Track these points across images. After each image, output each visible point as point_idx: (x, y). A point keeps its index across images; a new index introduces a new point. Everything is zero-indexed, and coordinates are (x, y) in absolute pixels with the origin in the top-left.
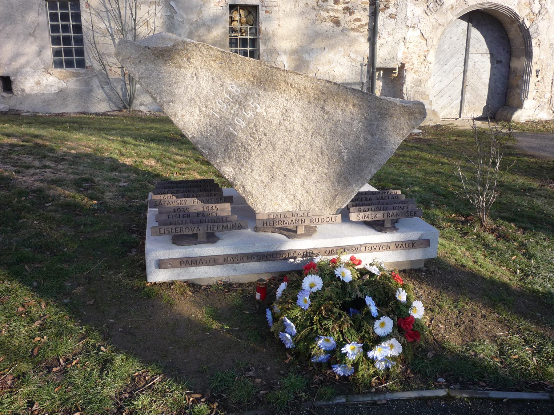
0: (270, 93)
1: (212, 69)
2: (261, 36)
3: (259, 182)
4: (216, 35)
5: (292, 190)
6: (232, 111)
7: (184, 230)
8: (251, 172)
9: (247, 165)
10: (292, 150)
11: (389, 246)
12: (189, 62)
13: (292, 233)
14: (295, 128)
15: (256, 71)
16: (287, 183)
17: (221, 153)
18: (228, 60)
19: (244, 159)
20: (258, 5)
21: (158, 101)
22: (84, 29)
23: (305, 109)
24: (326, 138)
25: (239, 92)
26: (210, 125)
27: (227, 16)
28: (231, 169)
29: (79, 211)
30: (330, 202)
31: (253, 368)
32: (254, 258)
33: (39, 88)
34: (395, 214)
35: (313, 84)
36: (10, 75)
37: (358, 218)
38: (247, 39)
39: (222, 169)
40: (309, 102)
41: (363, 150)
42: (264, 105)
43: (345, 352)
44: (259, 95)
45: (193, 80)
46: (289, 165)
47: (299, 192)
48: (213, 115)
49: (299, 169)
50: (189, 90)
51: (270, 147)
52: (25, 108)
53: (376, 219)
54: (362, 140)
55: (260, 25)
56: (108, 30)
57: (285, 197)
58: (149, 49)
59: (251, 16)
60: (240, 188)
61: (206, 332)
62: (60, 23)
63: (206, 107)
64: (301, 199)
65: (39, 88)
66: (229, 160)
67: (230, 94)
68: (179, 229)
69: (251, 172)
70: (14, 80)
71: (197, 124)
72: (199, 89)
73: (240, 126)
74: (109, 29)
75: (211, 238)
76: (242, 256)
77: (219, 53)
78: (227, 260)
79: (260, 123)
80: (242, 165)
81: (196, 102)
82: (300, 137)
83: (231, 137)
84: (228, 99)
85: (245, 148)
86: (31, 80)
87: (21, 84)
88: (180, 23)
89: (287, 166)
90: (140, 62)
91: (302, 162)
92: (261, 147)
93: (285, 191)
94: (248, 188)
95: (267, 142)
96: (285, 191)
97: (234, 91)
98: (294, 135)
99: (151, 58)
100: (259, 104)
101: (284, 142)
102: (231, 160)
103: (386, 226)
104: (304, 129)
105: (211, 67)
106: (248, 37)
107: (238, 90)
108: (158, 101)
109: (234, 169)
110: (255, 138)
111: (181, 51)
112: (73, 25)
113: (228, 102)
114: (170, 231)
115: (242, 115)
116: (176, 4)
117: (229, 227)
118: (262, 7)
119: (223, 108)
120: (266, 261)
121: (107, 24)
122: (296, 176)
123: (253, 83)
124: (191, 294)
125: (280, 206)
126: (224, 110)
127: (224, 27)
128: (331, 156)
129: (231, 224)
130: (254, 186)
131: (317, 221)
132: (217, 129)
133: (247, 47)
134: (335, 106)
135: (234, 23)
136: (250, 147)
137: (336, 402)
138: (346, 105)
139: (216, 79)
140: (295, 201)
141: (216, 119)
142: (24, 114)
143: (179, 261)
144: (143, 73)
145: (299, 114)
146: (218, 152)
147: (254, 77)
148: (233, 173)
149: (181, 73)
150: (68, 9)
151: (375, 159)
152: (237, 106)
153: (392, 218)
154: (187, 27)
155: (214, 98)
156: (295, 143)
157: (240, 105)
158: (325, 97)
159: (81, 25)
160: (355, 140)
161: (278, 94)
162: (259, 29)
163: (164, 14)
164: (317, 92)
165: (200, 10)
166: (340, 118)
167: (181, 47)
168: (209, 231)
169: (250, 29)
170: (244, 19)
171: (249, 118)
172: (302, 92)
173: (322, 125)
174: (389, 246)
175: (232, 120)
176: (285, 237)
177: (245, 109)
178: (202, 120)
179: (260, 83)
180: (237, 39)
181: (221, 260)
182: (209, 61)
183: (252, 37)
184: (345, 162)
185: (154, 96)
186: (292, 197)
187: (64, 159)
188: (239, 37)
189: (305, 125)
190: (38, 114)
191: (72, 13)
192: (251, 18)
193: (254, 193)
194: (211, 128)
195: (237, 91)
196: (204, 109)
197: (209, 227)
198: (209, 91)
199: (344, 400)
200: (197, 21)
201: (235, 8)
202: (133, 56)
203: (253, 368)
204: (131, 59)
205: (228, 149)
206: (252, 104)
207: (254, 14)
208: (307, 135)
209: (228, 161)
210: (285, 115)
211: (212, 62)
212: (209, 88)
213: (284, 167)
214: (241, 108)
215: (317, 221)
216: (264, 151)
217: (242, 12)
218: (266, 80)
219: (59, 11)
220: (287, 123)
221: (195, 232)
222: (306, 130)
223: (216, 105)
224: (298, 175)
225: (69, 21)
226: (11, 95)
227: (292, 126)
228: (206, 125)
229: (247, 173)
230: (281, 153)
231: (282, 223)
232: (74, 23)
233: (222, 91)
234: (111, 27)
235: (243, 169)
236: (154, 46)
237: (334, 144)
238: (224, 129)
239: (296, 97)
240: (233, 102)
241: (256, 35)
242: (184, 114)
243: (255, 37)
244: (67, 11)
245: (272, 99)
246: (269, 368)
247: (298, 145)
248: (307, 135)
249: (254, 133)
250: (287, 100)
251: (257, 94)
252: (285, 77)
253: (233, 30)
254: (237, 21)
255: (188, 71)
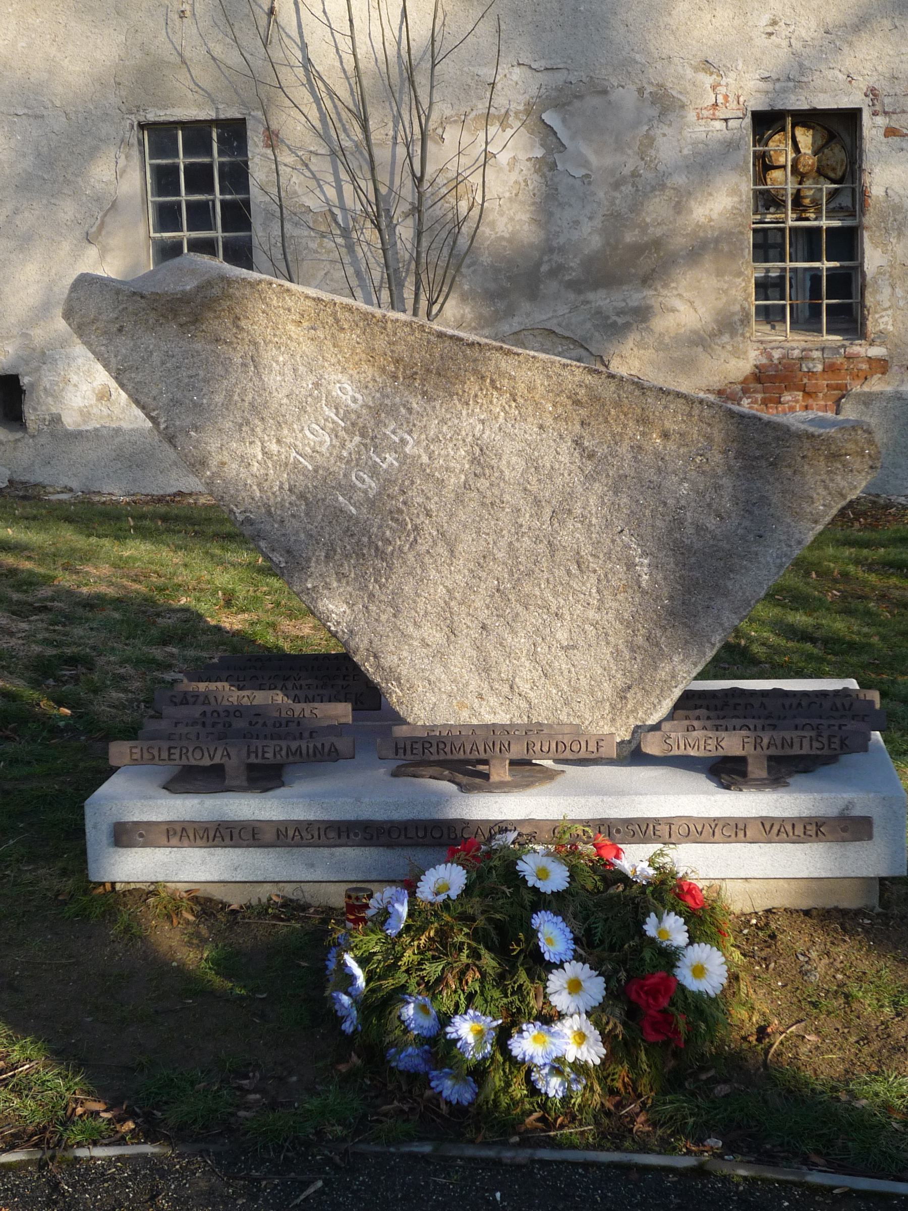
0: (437, 404)
1: (293, 345)
2: (869, 219)
3: (415, 643)
4: (702, 220)
5: (505, 669)
6: (345, 454)
7: (190, 754)
8: (395, 616)
9: (383, 597)
10: (500, 555)
11: (741, 826)
12: (238, 327)
13: (478, 780)
14: (507, 497)
15: (400, 348)
16: (490, 647)
17: (317, 562)
18: (331, 320)
19: (376, 581)
20: (859, 110)
21: (162, 426)
22: (257, 220)
23: (529, 445)
24: (590, 524)
25: (360, 402)
26: (290, 490)
27: (749, 149)
28: (344, 607)
29: (14, 731)
30: (613, 707)
31: (257, 1074)
32: (356, 835)
33: (105, 411)
34: (779, 742)
35: (549, 377)
36: (20, 370)
37: (666, 747)
38: (819, 229)
39: (320, 604)
40: (541, 427)
41: (693, 560)
42: (423, 437)
43: (454, 1036)
44: (410, 410)
45: (246, 372)
46: (492, 596)
47: (524, 673)
48: (297, 463)
49: (520, 609)
50: (236, 398)
51: (442, 549)
52: (64, 478)
53: (721, 752)
54: (691, 531)
55: (866, 179)
56: (333, 214)
57: (486, 686)
58: (142, 297)
59: (837, 149)
60: (368, 660)
61: (187, 998)
62: (184, 197)
63: (279, 441)
64: (531, 695)
65: (105, 411)
66: (339, 581)
67: (336, 409)
68: (177, 751)
69: (395, 616)
70: (32, 385)
71: (259, 485)
72: (260, 395)
73: (365, 492)
74: (337, 211)
75: (264, 777)
76: (323, 827)
77: (309, 303)
78: (284, 836)
79: (413, 483)
80: (371, 596)
81: (253, 430)
82: (520, 520)
83: (341, 519)
84: (334, 422)
85: (377, 548)
86: (84, 387)
87: (50, 400)
88: (578, 183)
89: (488, 600)
90: (120, 330)
91: (527, 589)
92: (418, 547)
93: (487, 670)
94: (389, 660)
95: (435, 533)
96: (487, 670)
97: (347, 399)
98: (505, 517)
99: (147, 320)
100: (410, 432)
101: (478, 533)
102: (344, 581)
103: (751, 776)
104: (530, 499)
105: (290, 338)
106: (825, 223)
107: (358, 396)
108: (162, 426)
109: (351, 606)
110: (403, 524)
111: (217, 300)
112: (223, 202)
113: (333, 430)
114: (156, 753)
115: (370, 463)
116: (564, 121)
117: (304, 751)
118: (875, 114)
119: (321, 443)
120: (389, 846)
121: (331, 193)
122: (513, 632)
123: (395, 377)
124: (191, 918)
125: (474, 713)
126: (324, 449)
127: (734, 191)
128: (606, 576)
129: (311, 746)
130: (405, 654)
131: (545, 749)
132: (306, 499)
133: (819, 260)
134: (613, 435)
135: (776, 174)
136: (390, 548)
137: (405, 1149)
138: (643, 434)
139: (302, 369)
140: (516, 699)
141: (304, 471)
142: (54, 497)
143: (165, 827)
144: (125, 356)
145: (514, 459)
146: (308, 560)
147: (397, 361)
148: (349, 617)
149: (219, 356)
150: (210, 153)
151: (729, 584)
152: (357, 439)
153: (769, 752)
154: (601, 194)
155: (299, 420)
156: (507, 538)
157: (363, 435)
158: (583, 412)
159: (247, 203)
160: (670, 531)
161: (459, 406)
162: (864, 194)
163: (522, 156)
164: (563, 398)
165: (647, 136)
166: (627, 469)
167: (216, 291)
168: (253, 760)
169: (833, 194)
170: (808, 159)
171: (386, 471)
172: (521, 401)
173: (580, 489)
174: (741, 826)
175: (345, 475)
176: (454, 787)
177: (376, 447)
178: (271, 477)
179: (413, 377)
180: (782, 230)
181: (270, 836)
182: (284, 324)
183: (836, 223)
184: (644, 593)
185: (153, 414)
186: (506, 688)
187: (46, 607)
188: (790, 223)
189: (534, 488)
190: (96, 498)
191: (221, 165)
192: (836, 155)
193: (404, 673)
194: (294, 498)
195: (355, 400)
196: (274, 447)
197: (253, 749)
198: (285, 401)
199: (427, 1148)
200: (635, 174)
201: (778, 126)
202: (104, 317)
203: (257, 1074)
204: (98, 324)
205: (335, 551)
206: (394, 432)
207: (848, 140)
208: (538, 516)
209: (335, 584)
210: (479, 463)
211: (291, 327)
212: (285, 392)
213: (478, 604)
214: (365, 445)
215: (545, 749)
216: (427, 560)
217: (805, 138)
218: (428, 371)
219: (182, 161)
220: (483, 483)
221: (217, 760)
222: (537, 502)
223: (305, 436)
224: (518, 626)
225: (211, 190)
226: (19, 435)
227: (496, 491)
228: (281, 488)
229: (383, 617)
230: (471, 566)
231: (448, 749)
232: (228, 197)
233: (318, 399)
234: (343, 208)
235: (372, 607)
236: (154, 290)
237: (613, 541)
238: (324, 500)
239: (506, 413)
240: (344, 429)
241: (853, 215)
242: (226, 459)
243: (848, 223)
244: (206, 160)
245: (443, 421)
246: (294, 1079)
247: (517, 545)
248: (538, 516)
249: (400, 511)
250: (483, 422)
251: (404, 406)
252: (475, 360)
253: (767, 200)
254: (784, 167)
255: (235, 349)
